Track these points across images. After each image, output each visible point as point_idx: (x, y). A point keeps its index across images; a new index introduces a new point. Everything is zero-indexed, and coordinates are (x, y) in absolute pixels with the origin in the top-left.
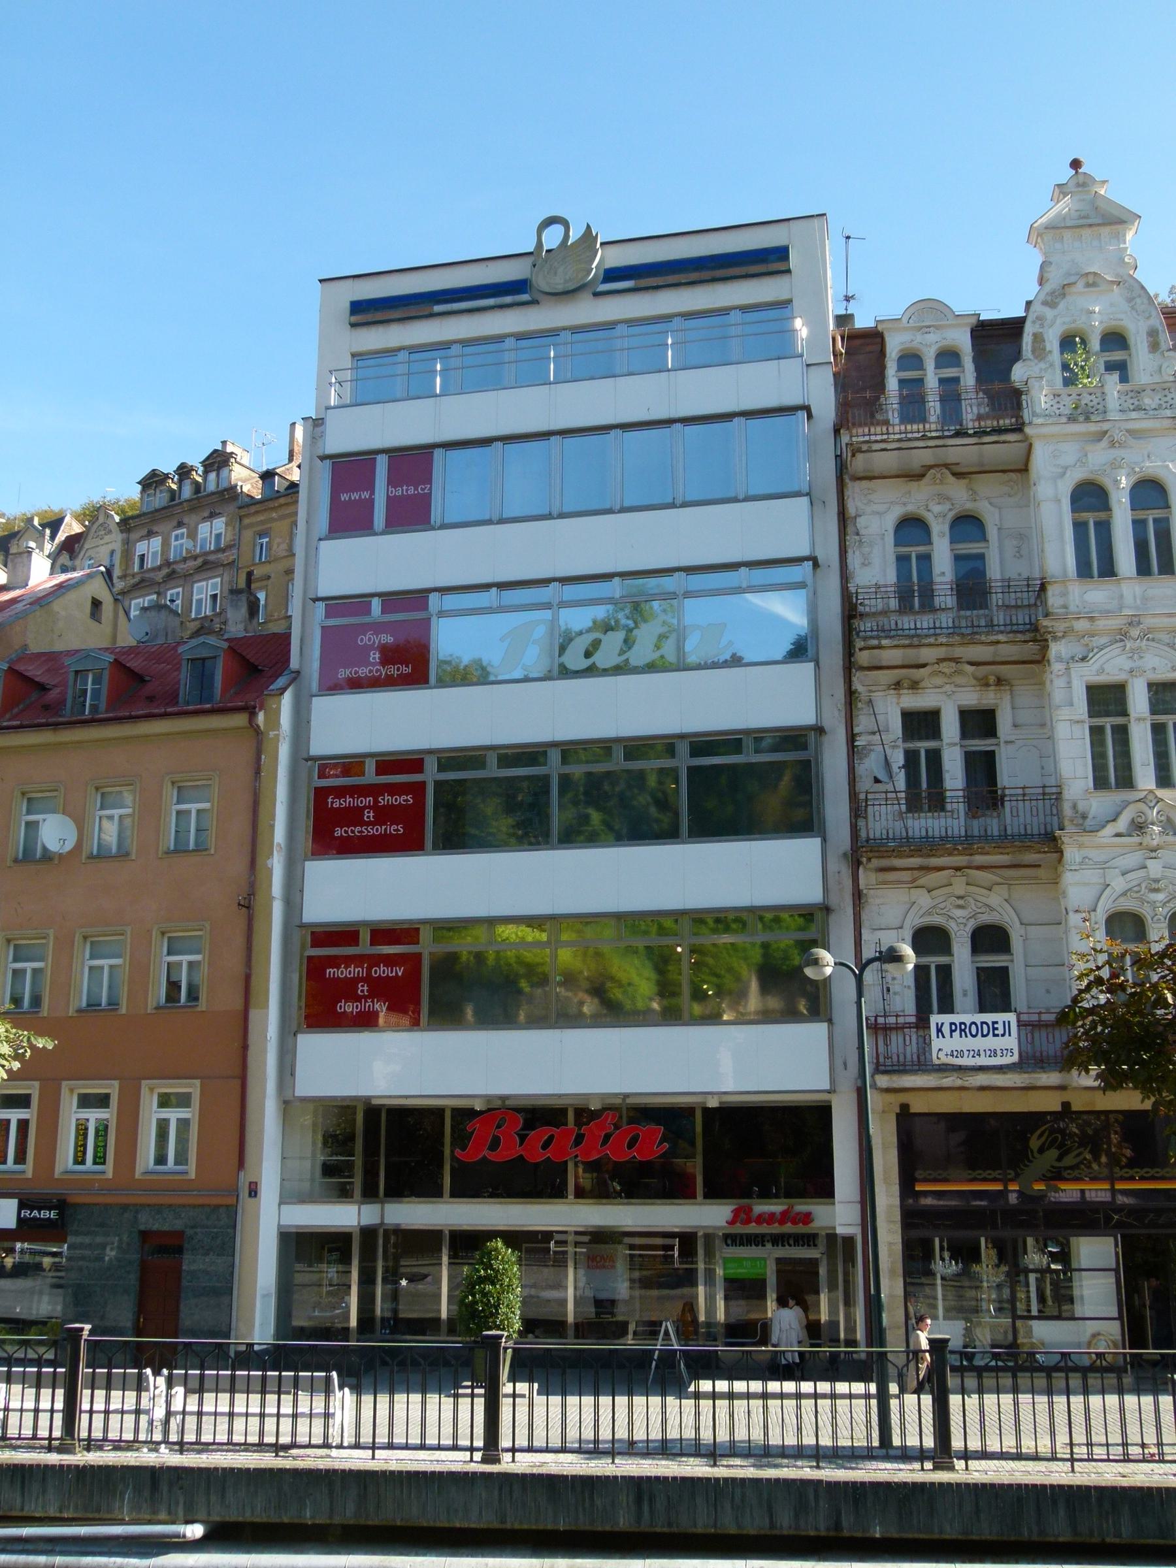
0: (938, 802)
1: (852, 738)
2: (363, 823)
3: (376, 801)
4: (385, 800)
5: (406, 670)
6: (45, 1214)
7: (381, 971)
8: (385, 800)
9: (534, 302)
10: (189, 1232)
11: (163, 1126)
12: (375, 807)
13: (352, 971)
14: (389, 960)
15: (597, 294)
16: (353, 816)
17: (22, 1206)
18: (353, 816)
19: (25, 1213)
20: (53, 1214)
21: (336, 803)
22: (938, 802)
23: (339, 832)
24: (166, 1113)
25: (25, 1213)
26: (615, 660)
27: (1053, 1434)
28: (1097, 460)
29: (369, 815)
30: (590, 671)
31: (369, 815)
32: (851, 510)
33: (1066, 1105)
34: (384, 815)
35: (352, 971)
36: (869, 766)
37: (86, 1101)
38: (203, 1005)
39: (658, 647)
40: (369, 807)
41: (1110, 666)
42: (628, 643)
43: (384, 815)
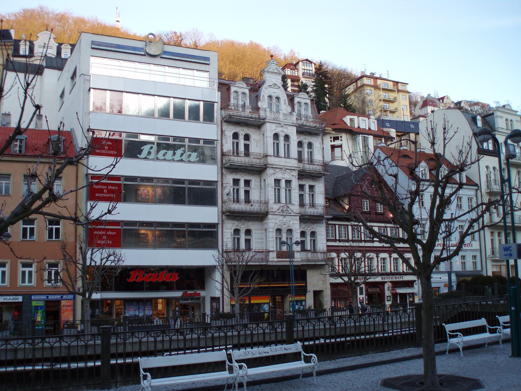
0: (238, 201)
1: (222, 184)
3: (107, 187)
4: (110, 187)
5: (115, 153)
7: (110, 233)
8: (110, 187)
9: (145, 55)
11: (24, 273)
12: (107, 189)
13: (101, 233)
14: (112, 230)
15: (162, 58)
16: (101, 191)
18: (101, 191)
22: (238, 201)
23: (97, 195)
24: (24, 269)
26: (171, 158)
27: (413, 317)
28: (279, 130)
29: (105, 191)
31: (105, 191)
32: (224, 129)
33: (279, 269)
34: (110, 191)
35: (101, 233)
36: (226, 191)
37: (25, 265)
38: (35, 237)
41: (279, 176)
42: (174, 154)
43: (110, 191)
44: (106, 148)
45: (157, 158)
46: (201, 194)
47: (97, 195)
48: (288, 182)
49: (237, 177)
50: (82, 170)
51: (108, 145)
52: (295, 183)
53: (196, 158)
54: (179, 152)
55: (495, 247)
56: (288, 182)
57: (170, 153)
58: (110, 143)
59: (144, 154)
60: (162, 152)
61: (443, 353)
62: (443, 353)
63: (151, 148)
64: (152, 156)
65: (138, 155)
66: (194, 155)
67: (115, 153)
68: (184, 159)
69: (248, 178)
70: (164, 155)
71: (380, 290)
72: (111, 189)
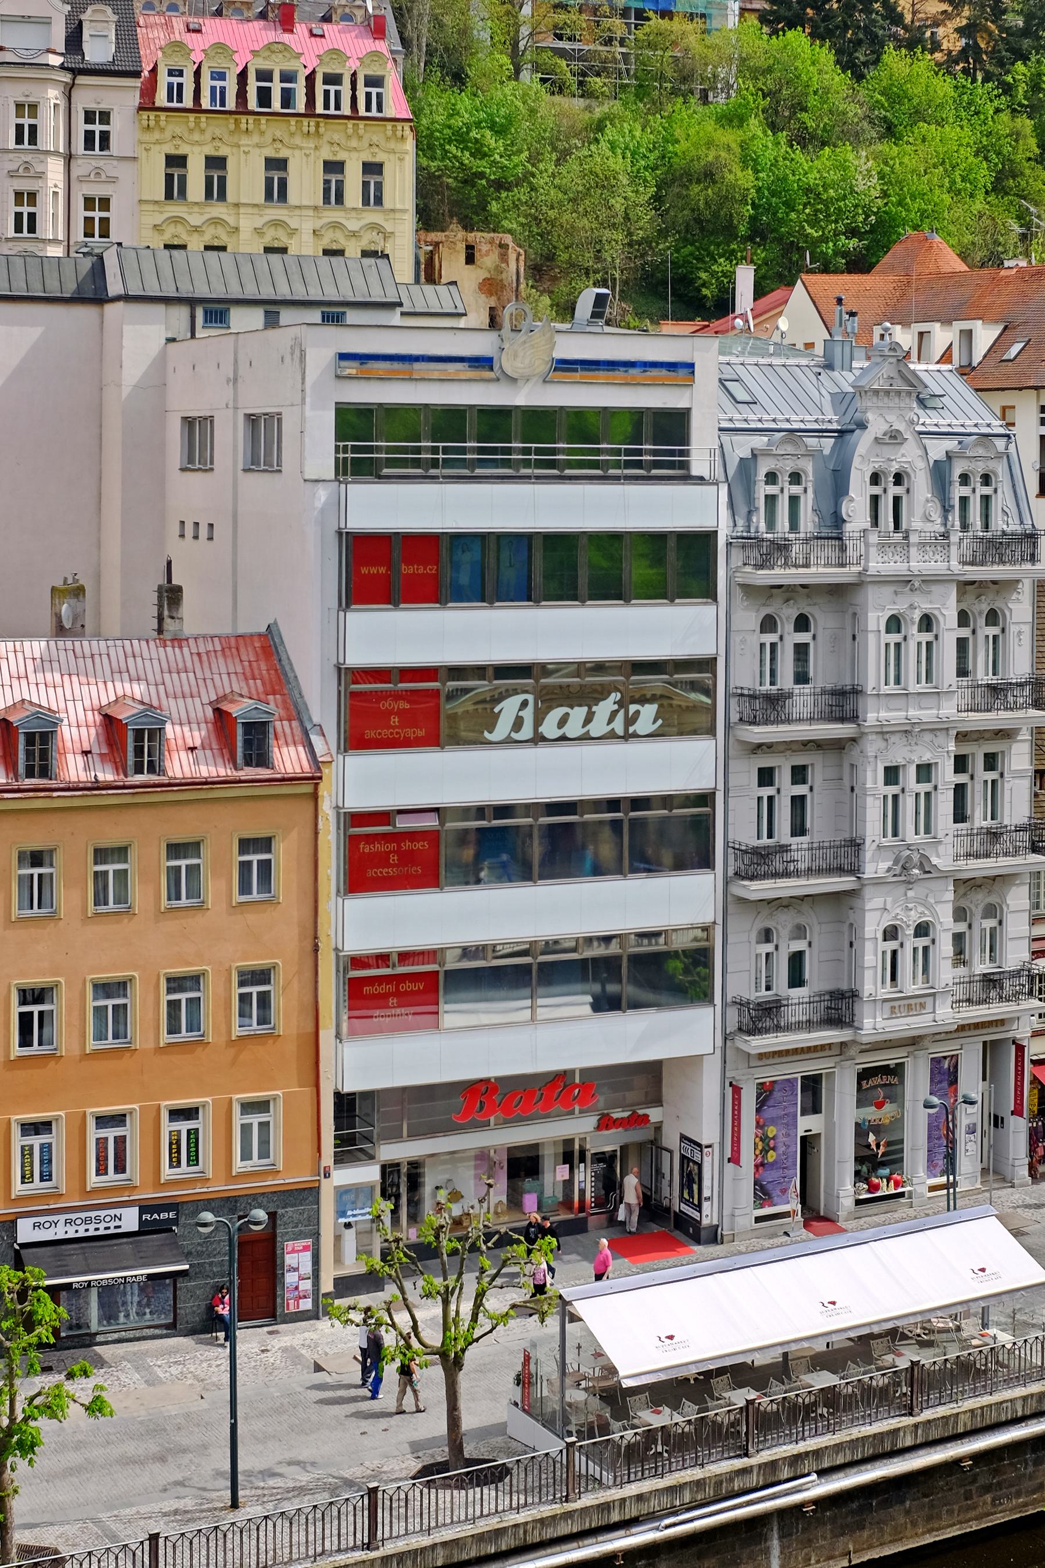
2: (389, 866)
3: (399, 846)
4: (407, 845)
6: (164, 1216)
10: (280, 1211)
16: (382, 860)
17: (143, 1210)
19: (146, 1217)
20: (172, 1215)
21: (365, 848)
24: (103, 1133)
25: (146, 1217)
26: (580, 732)
29: (394, 859)
30: (563, 738)
31: (394, 859)
39: (610, 721)
40: (394, 852)
41: (899, 754)
44: (395, 720)
45: (544, 739)
46: (661, 835)
47: (371, 873)
48: (925, 771)
49: (766, 762)
50: (326, 807)
51: (400, 713)
52: (947, 776)
53: (654, 722)
54: (605, 707)
55: (456, 1014)
56: (925, 771)
57: (578, 713)
58: (404, 705)
59: (502, 729)
60: (557, 713)
61: (193, 318)
62: (193, 318)
63: (524, 704)
64: (527, 732)
65: (486, 734)
66: (649, 711)
67: (421, 733)
68: (620, 731)
69: (800, 760)
70: (563, 722)
71: (358, 572)
72: (412, 852)
